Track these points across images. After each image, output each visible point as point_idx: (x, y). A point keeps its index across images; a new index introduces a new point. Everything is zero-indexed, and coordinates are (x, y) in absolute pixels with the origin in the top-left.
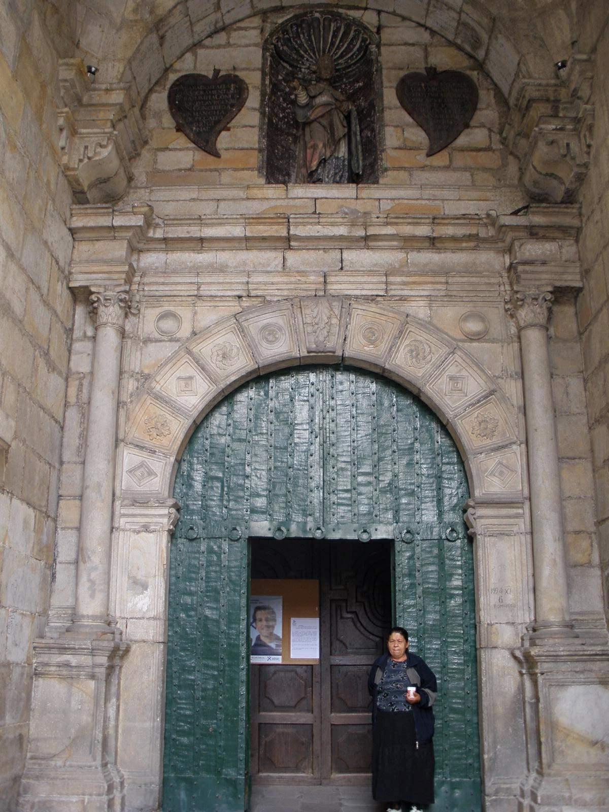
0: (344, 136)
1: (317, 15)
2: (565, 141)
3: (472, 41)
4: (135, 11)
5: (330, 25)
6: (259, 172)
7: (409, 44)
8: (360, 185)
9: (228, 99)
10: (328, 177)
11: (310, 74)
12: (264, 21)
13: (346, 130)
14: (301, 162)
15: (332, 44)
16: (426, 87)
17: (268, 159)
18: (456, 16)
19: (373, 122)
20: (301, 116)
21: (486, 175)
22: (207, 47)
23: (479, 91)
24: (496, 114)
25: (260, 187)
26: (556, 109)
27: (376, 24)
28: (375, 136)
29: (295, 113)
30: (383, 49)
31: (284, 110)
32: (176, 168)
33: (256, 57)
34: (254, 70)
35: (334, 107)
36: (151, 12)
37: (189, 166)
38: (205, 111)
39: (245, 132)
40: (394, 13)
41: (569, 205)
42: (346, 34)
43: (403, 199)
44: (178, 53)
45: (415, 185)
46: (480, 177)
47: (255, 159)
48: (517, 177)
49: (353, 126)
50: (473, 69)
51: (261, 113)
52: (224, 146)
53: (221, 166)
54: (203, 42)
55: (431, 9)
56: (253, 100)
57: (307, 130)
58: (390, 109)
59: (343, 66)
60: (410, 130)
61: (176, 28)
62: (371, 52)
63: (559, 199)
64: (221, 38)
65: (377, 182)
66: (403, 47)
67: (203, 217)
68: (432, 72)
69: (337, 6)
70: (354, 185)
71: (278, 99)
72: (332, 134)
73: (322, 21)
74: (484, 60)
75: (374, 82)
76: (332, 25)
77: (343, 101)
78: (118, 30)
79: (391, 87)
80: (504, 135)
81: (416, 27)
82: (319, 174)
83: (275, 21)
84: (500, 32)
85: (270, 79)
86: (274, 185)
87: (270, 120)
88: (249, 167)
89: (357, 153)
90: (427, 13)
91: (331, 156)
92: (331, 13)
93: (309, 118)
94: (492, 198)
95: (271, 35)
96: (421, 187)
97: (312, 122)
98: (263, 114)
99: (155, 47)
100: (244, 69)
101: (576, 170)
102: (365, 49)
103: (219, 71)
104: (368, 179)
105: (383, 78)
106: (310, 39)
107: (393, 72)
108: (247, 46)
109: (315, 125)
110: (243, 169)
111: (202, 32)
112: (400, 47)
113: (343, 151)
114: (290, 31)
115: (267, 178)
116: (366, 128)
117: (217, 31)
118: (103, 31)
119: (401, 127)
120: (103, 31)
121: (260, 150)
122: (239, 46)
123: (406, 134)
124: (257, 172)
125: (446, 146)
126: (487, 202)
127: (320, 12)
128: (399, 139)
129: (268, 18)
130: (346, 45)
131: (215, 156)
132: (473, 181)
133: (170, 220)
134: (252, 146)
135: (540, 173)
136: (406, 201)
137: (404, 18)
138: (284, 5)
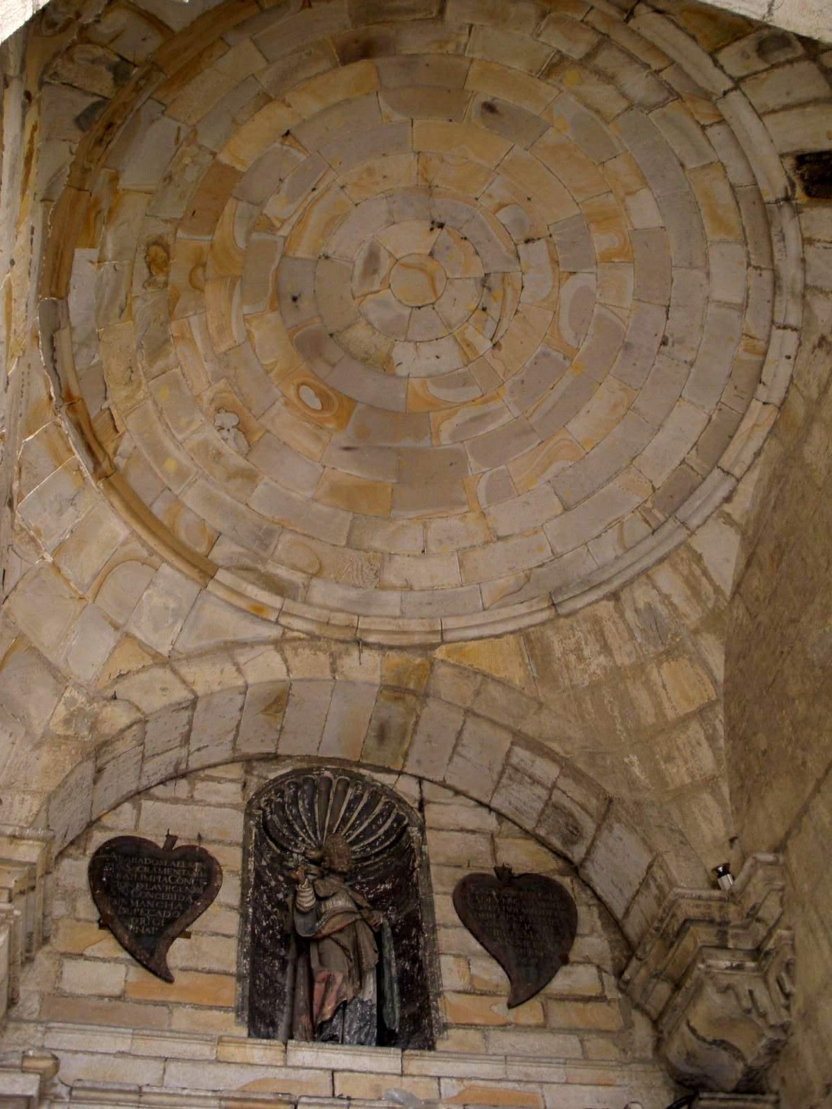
1: (327, 774)
2: (747, 988)
3: (566, 832)
4: (67, 722)
5: (345, 792)
6: (238, 1016)
9: (190, 886)
10: (349, 1032)
12: (246, 772)
16: (498, 896)
18: (544, 793)
20: (303, 926)
21: (602, 1042)
22: (158, 799)
23: (578, 908)
24: (606, 945)
25: (239, 1042)
26: (723, 935)
28: (421, 969)
30: (428, 834)
32: (93, 992)
34: (230, 844)
36: (92, 728)
37: (117, 991)
38: (151, 900)
39: (213, 943)
40: (443, 784)
41: (760, 1097)
42: (368, 808)
43: (476, 1078)
45: (494, 1055)
46: (597, 1044)
47: (231, 992)
48: (650, 1047)
50: (562, 874)
51: (242, 915)
53: (172, 999)
54: (152, 790)
55: (504, 781)
56: (229, 891)
58: (445, 926)
59: (358, 856)
61: (121, 759)
62: (409, 837)
63: (731, 1086)
65: (432, 1047)
66: (459, 834)
67: (145, 1089)
68: (505, 875)
69: (359, 765)
74: (584, 860)
76: (350, 791)
78: (38, 746)
79: (445, 893)
80: (627, 976)
81: (475, 806)
82: (335, 1028)
83: (265, 774)
84: (619, 821)
88: (221, 1004)
89: (392, 995)
91: (354, 998)
92: (350, 774)
94: (618, 1082)
95: (258, 794)
96: (506, 1059)
97: (325, 937)
98: (244, 916)
99: (86, 784)
100: (214, 841)
101: (770, 1034)
102: (400, 831)
104: (408, 1042)
105: (433, 878)
106: (311, 810)
107: (447, 871)
109: (328, 944)
110: (211, 1008)
112: (452, 833)
113: (370, 992)
118: (13, 743)
120: (13, 743)
121: (240, 978)
122: (209, 805)
123: (474, 971)
125: (537, 992)
126: (611, 1089)
129: (253, 768)
130: (366, 824)
132: (584, 1052)
133: (84, 1089)
134: (226, 969)
135: (704, 1040)
136: (481, 1083)
137: (457, 793)
138: (280, 752)
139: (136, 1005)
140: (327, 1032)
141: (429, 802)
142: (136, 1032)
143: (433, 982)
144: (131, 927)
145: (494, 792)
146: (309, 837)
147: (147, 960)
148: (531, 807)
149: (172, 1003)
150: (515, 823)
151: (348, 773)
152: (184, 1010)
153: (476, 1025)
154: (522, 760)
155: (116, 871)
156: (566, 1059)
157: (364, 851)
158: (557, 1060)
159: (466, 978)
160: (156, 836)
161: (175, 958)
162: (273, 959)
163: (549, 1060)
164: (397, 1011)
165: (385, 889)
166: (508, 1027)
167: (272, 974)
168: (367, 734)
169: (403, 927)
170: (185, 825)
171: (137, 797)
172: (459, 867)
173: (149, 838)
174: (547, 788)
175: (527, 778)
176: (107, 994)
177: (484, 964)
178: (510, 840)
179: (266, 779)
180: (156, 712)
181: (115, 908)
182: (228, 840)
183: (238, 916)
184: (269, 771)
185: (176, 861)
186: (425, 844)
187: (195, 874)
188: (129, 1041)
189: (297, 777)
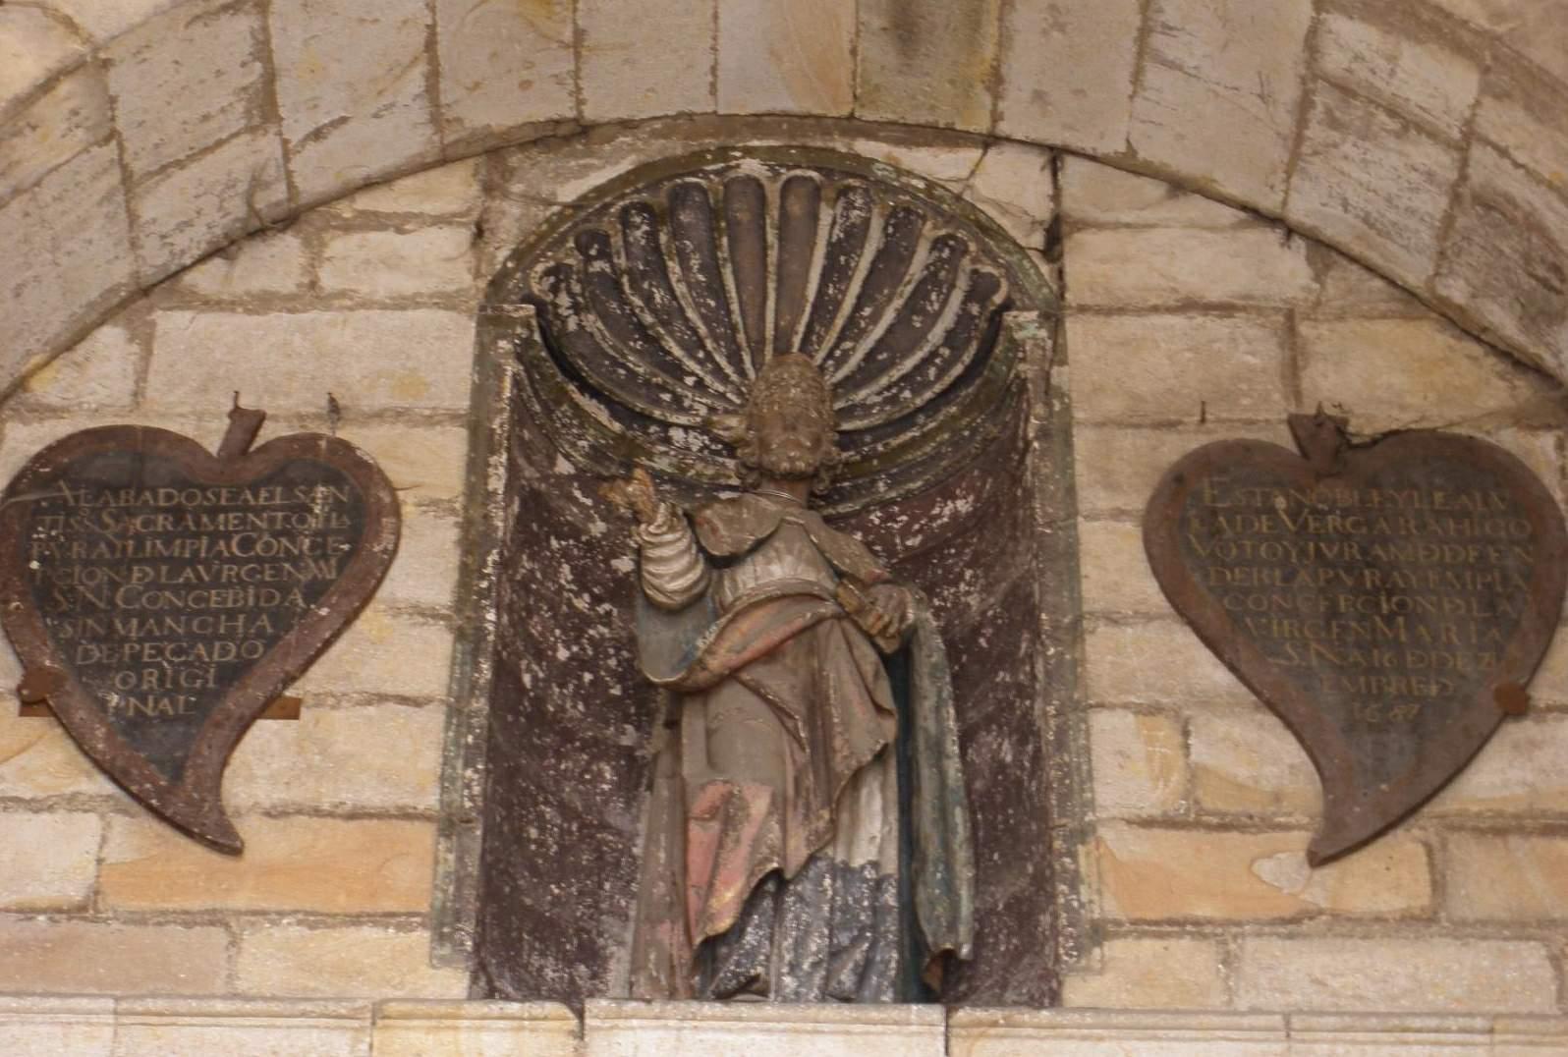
0: (880, 757)
1: (751, 166)
5: (814, 218)
6: (441, 938)
7: (1207, 308)
8: (963, 1014)
9: (295, 560)
10: (794, 968)
11: (707, 454)
12: (488, 189)
13: (890, 728)
14: (661, 888)
15: (824, 308)
16: (1294, 515)
17: (486, 867)
18: (1442, 162)
19: (1024, 691)
22: (209, 304)
25: (440, 1014)
27: (1043, 210)
28: (1037, 758)
29: (632, 642)
30: (1075, 330)
31: (575, 627)
33: (445, 357)
34: (430, 421)
35: (828, 608)
37: (75, 893)
38: (176, 613)
39: (374, 725)
40: (1129, 164)
42: (892, 258)
44: (56, 325)
45: (1254, 1011)
47: (421, 868)
49: (926, 707)
50: (1523, 420)
51: (460, 635)
52: (266, 793)
53: (240, 901)
54: (188, 278)
55: (1316, 132)
56: (424, 565)
57: (693, 725)
58: (1113, 619)
59: (876, 419)
60: (1221, 726)
61: (47, 193)
62: (1015, 345)
64: (279, 262)
65: (1054, 999)
66: (1177, 321)
68: (1326, 442)
69: (851, 126)
70: (935, 1013)
71: (551, 573)
72: (820, 745)
73: (773, 191)
75: (1029, 494)
76: (826, 215)
77: (878, 580)
79: (1118, 514)
82: (751, 955)
83: (545, 190)
85: (512, 468)
86: (514, 1008)
87: (505, 672)
89: (946, 845)
90: (1295, 155)
91: (812, 859)
93: (701, 664)
95: (523, 255)
98: (469, 637)
100: (379, 415)
102: (988, 331)
103: (260, 418)
105: (1080, 468)
106: (717, 289)
107: (1127, 441)
108: (402, 303)
109: (732, 697)
110: (356, 920)
111: (183, 226)
113: (872, 835)
114: (617, 241)
115: (480, 970)
116: (989, 720)
117: (258, 229)
119: (1175, 713)
121: (449, 824)
122: (366, 304)
123: (1200, 752)
124: (427, 935)
125: (1413, 810)
127: (767, 155)
128: (1163, 774)
129: (509, 174)
130: (889, 316)
131: (214, 846)
134: (407, 800)
137: (1178, 186)
138: (590, 113)
139: (131, 929)
140: (729, 968)
141: (1083, 225)
142: (124, 1005)
143: (1064, 798)
144: (114, 699)
145: (1289, 174)
146: (718, 372)
147: (160, 793)
148: (1411, 211)
149: (238, 913)
150: (1370, 269)
151: (820, 160)
152: (276, 932)
153: (1197, 923)
154: (1358, 58)
155: (69, 538)
156: (1497, 1016)
157: (893, 400)
158: (1463, 1022)
159: (1175, 778)
160: (200, 417)
161: (251, 778)
162: (594, 758)
163: (1433, 1022)
164: (965, 893)
165: (955, 515)
166: (1307, 926)
167: (588, 808)
168: (858, 23)
169: (998, 629)
170: (291, 375)
171: (142, 303)
172: (1171, 425)
173: (173, 427)
174: (1449, 145)
175: (1382, 117)
176: (44, 904)
177: (1237, 731)
178: (1353, 325)
179: (549, 203)
180: (131, 29)
181: (70, 646)
182: (423, 406)
183: (449, 637)
184: (561, 177)
185: (255, 489)
186: (1063, 362)
187: (313, 523)
188: (108, 1032)
189: (654, 186)
